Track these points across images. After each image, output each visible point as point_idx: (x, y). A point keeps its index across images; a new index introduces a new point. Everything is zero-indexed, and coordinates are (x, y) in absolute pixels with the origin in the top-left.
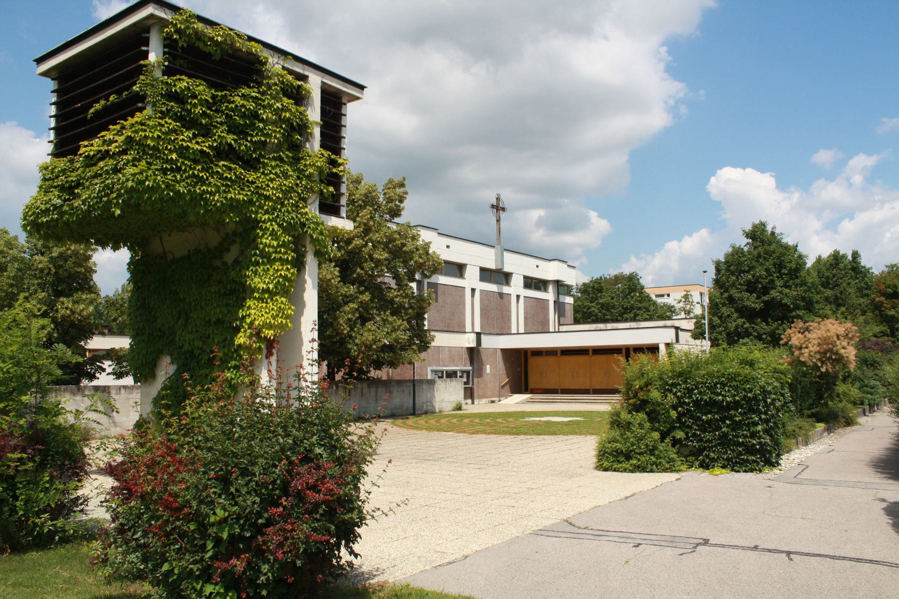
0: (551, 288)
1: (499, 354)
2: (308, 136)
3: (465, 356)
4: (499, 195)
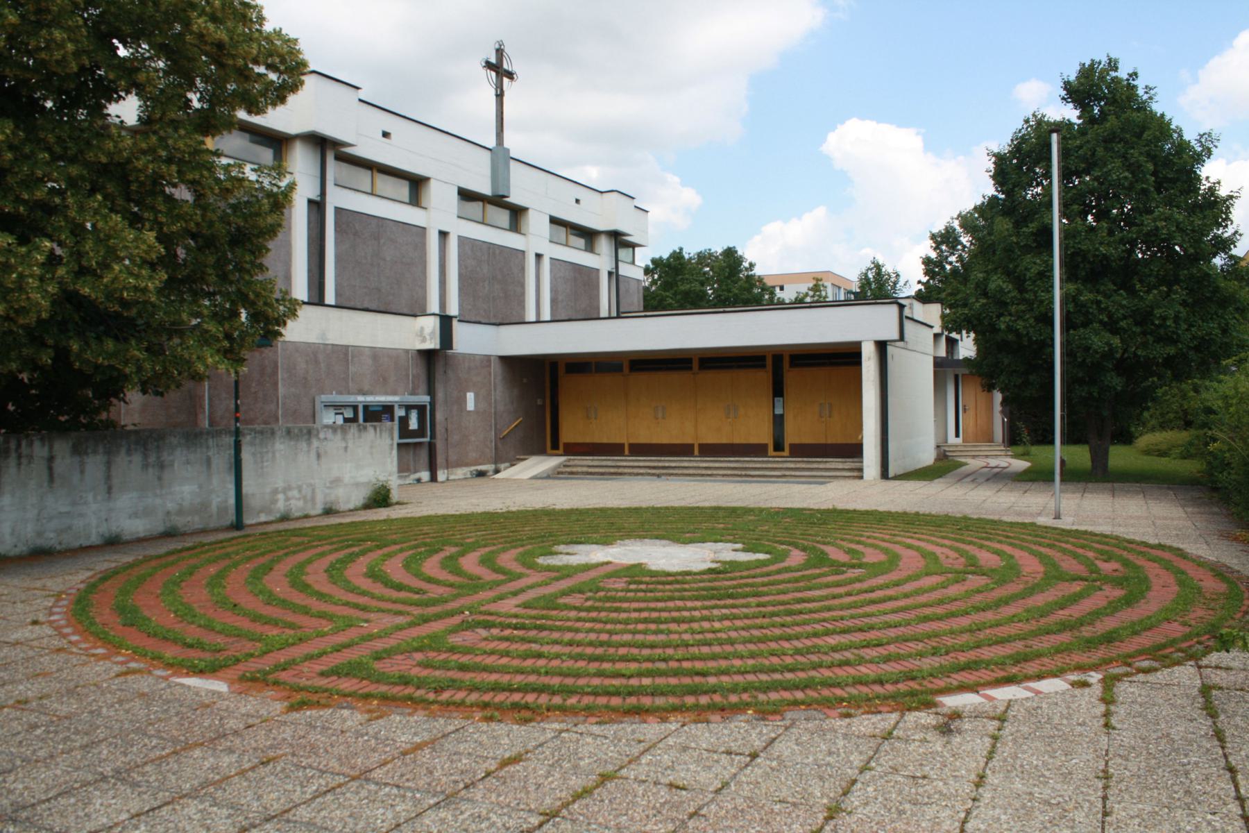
0: (604, 245)
1: (496, 368)
2: (250, 112)
3: (416, 370)
4: (501, 44)
